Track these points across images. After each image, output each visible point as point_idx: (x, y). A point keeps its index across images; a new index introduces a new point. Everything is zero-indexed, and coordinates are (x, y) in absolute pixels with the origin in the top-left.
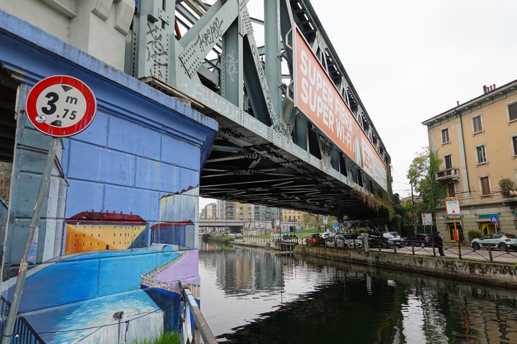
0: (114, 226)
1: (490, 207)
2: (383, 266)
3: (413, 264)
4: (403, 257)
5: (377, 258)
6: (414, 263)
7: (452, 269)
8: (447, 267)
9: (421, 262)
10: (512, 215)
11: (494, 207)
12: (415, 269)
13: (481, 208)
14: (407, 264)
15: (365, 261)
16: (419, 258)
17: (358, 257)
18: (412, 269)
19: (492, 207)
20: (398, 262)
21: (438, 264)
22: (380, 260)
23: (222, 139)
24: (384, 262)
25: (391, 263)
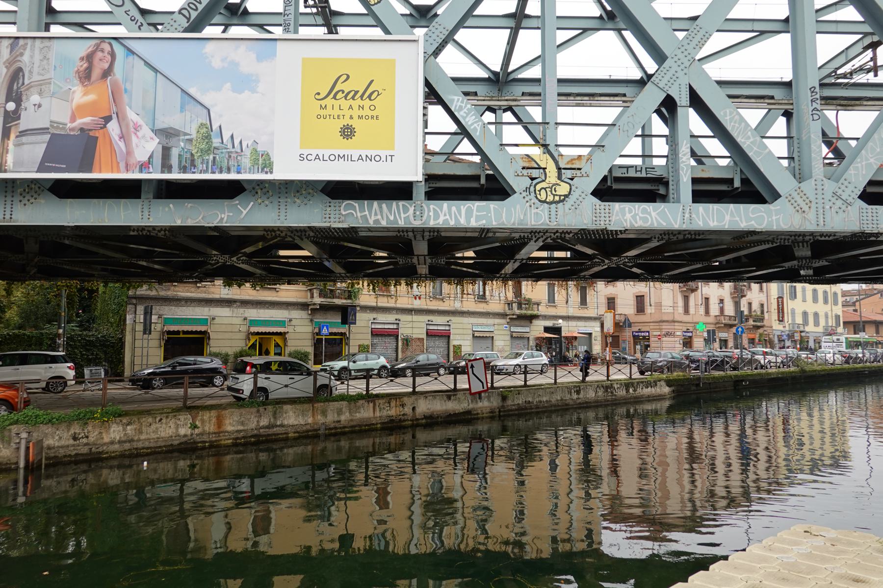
0: (612, 78)
1: (273, 308)
2: (516, 412)
3: (568, 397)
4: (552, 390)
5: (504, 398)
6: (569, 396)
7: (612, 392)
8: (607, 391)
9: (578, 392)
10: (310, 324)
11: (281, 308)
12: (571, 402)
13: (256, 308)
14: (559, 398)
15: (469, 412)
16: (575, 387)
17: (444, 408)
18: (567, 405)
19: (278, 309)
20: (544, 399)
21: (598, 390)
22: (509, 402)
23: (658, 244)
24: (518, 404)
25: (532, 402)
